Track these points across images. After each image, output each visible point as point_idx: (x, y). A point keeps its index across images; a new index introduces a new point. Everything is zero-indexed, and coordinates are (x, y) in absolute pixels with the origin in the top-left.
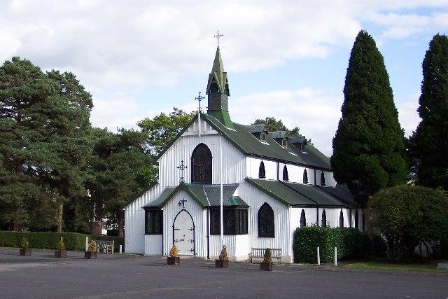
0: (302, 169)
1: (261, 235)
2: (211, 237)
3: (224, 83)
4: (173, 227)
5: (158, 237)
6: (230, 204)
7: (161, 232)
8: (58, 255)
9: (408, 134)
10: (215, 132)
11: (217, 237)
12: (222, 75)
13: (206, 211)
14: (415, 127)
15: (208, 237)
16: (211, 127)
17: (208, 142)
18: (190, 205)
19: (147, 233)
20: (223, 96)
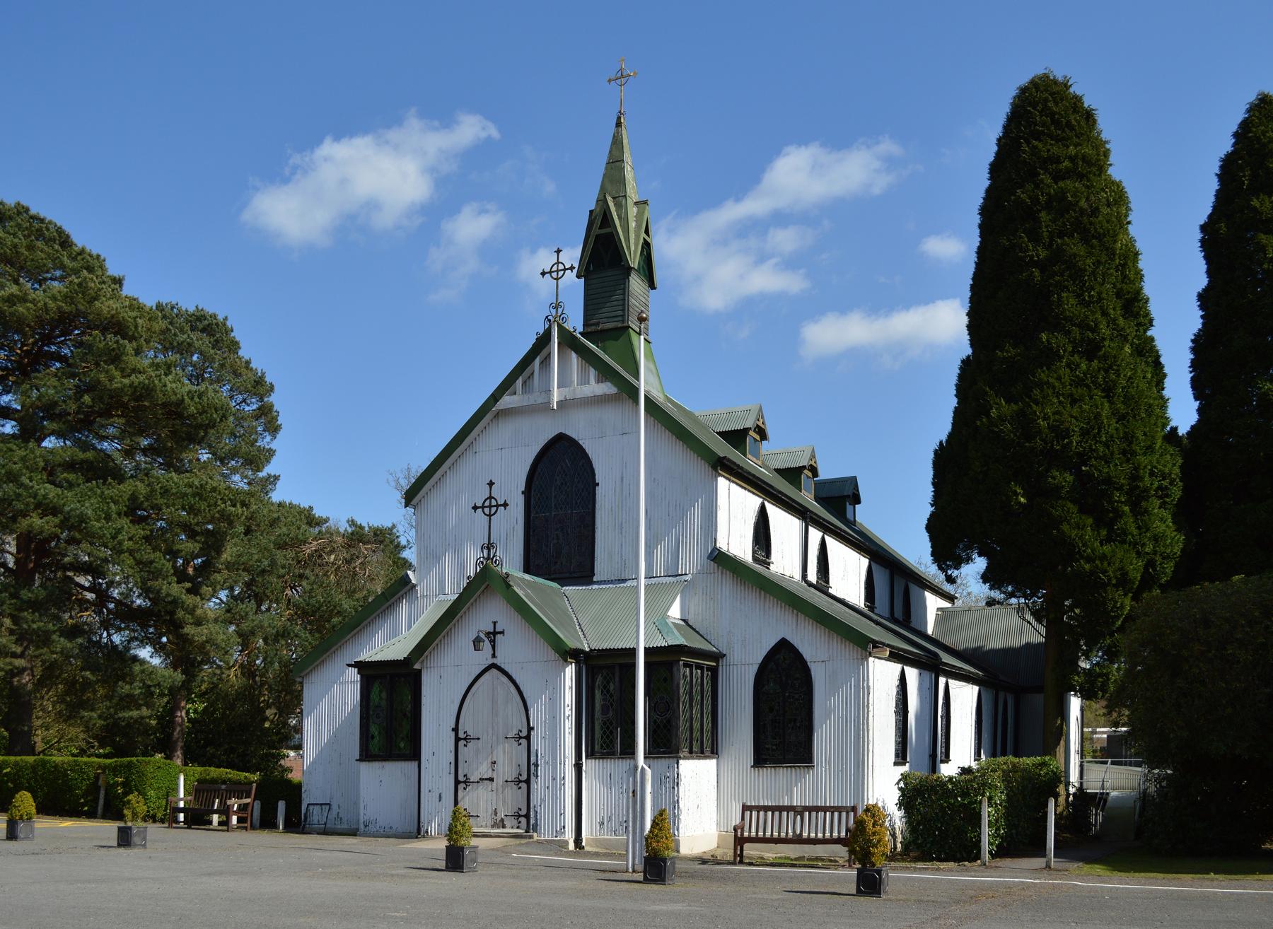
0: (896, 668)
1: (762, 758)
2: (588, 765)
3: (637, 237)
4: (456, 730)
5: (412, 766)
6: (660, 642)
7: (413, 753)
8: (125, 839)
9: (1034, 633)
10: (607, 388)
11: (616, 767)
12: (633, 211)
13: (570, 671)
14: (1193, 418)
15: (578, 767)
16: (592, 373)
17: (579, 428)
18: (518, 649)
19: (367, 755)
20: (636, 284)
